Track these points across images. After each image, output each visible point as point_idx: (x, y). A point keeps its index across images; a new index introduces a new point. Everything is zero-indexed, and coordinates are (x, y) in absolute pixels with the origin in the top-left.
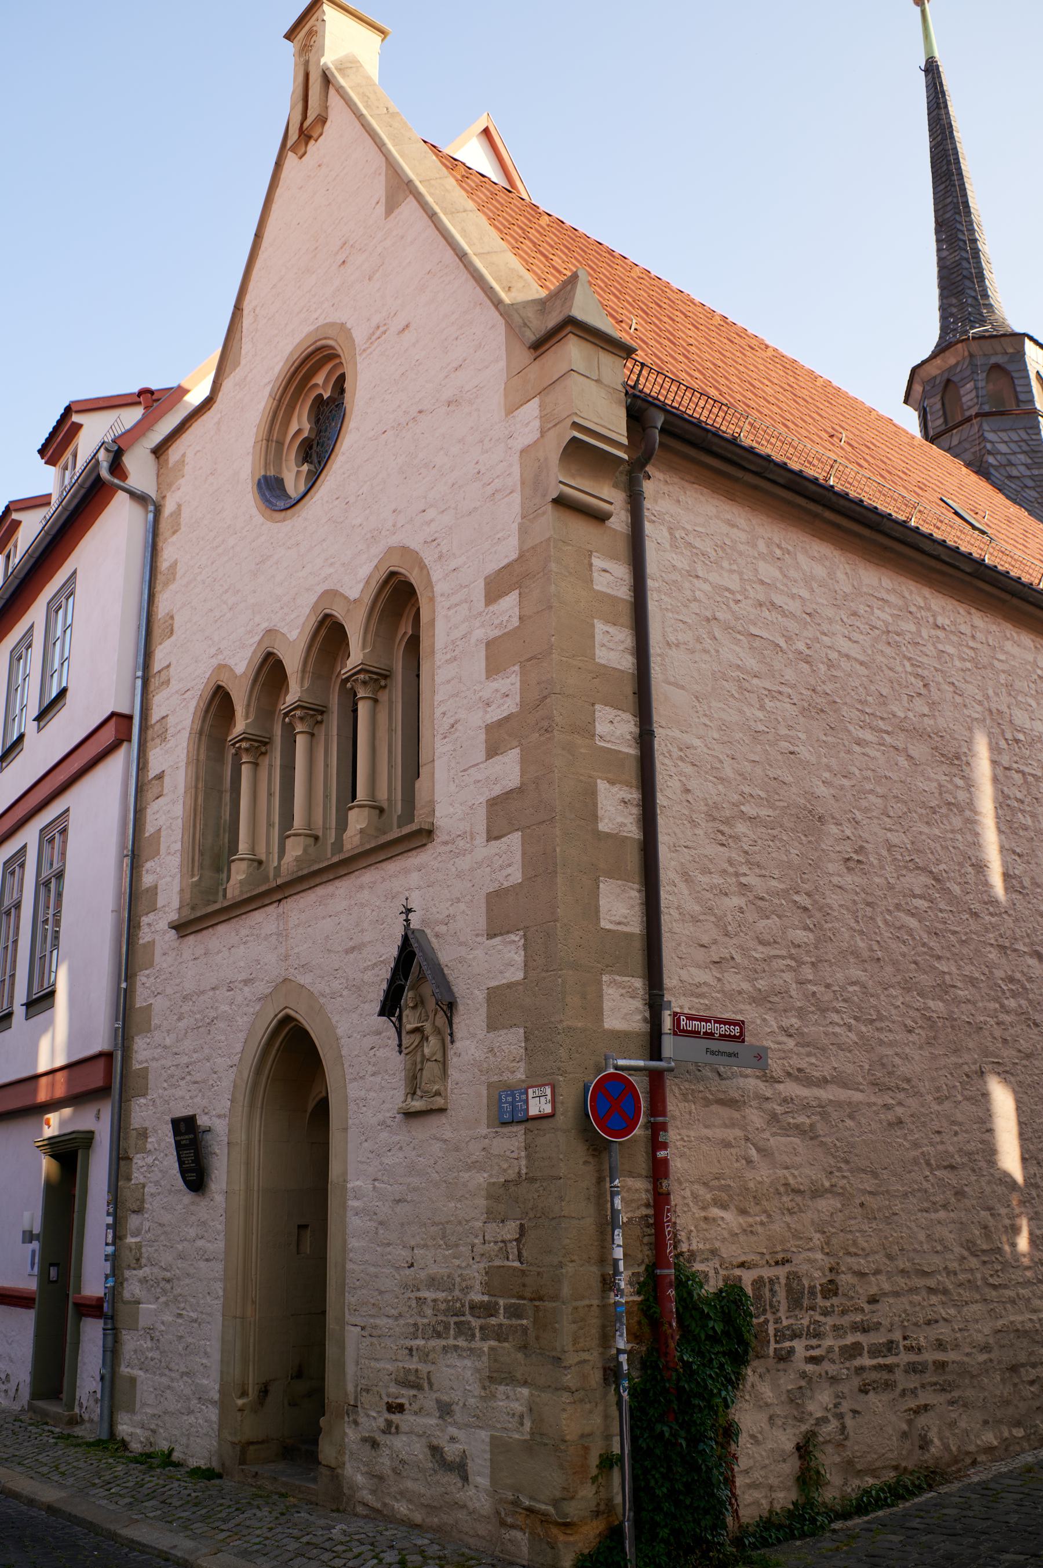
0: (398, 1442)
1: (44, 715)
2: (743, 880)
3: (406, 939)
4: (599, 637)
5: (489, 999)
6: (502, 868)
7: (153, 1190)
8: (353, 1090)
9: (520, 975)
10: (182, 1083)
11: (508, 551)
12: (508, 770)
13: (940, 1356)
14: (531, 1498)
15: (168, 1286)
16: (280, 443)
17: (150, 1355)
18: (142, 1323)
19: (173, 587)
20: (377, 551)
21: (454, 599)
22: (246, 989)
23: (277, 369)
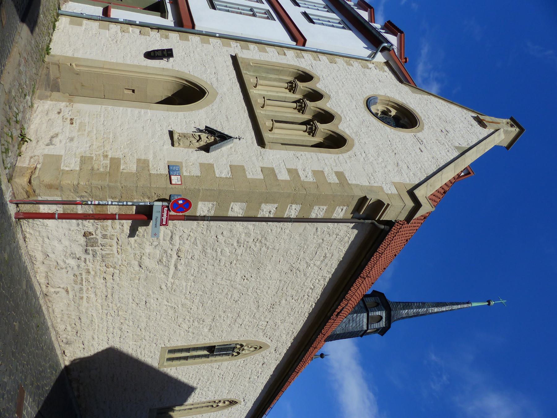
0: (60, 121)
1: (305, 14)
2: (242, 246)
3: (231, 137)
4: (322, 207)
5: (210, 164)
6: (252, 171)
7: (148, 39)
8: (181, 114)
9: (217, 176)
10: (184, 53)
11: (352, 181)
12: (283, 176)
13: (85, 298)
14: (40, 169)
15: (114, 41)
16: (388, 105)
17: (90, 32)
18: (102, 31)
19: (345, 64)
20: (353, 136)
21: (337, 161)
22: (215, 79)
23: (411, 106)
